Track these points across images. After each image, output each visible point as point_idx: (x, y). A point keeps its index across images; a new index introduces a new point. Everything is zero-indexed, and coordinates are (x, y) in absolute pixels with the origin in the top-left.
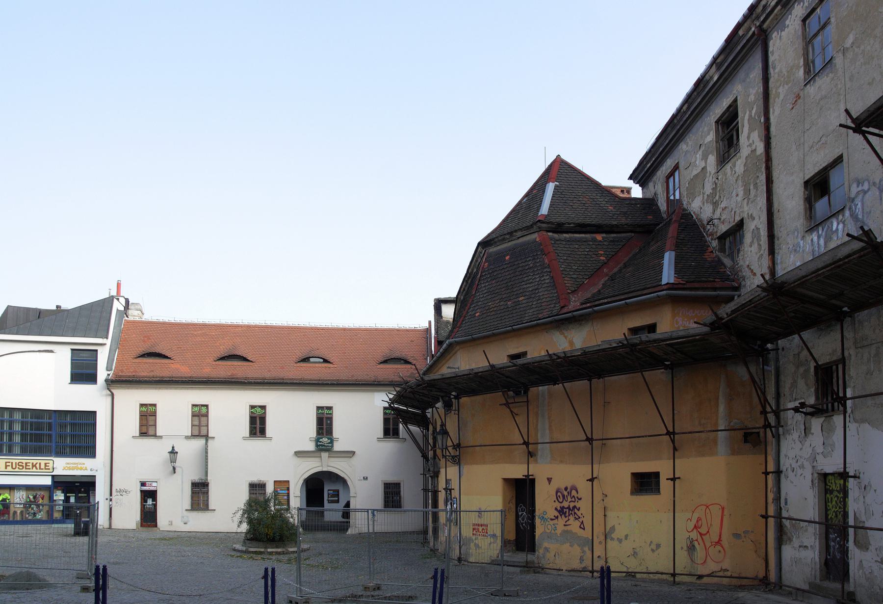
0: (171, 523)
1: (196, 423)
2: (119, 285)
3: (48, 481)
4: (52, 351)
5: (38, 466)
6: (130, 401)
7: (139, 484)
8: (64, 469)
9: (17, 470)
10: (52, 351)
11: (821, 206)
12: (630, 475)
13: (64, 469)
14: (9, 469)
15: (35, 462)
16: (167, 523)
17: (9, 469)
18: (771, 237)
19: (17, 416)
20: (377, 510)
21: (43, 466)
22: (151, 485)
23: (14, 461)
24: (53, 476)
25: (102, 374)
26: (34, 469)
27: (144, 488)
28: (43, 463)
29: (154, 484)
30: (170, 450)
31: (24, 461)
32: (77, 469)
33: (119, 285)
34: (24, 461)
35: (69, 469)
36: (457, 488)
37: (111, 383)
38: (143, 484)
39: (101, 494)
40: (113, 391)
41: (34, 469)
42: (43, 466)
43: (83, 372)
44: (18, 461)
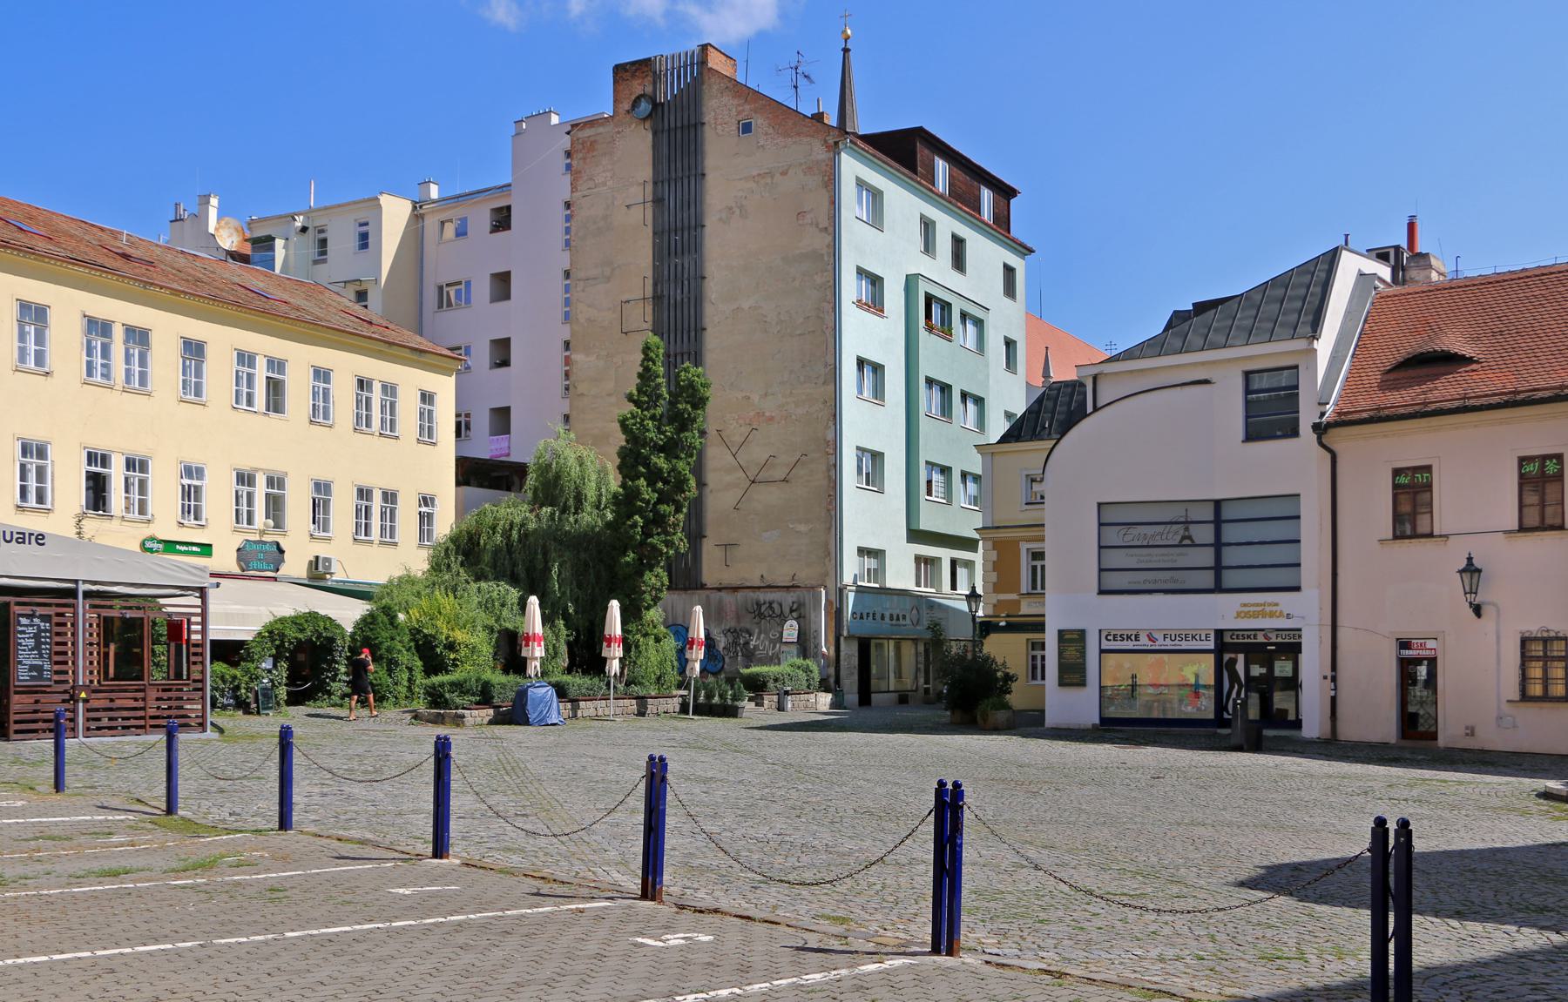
0: (1471, 732)
1: (1406, 508)
2: (1411, 227)
4: (1206, 382)
6: (1374, 460)
7: (1394, 646)
8: (1238, 615)
10: (1206, 382)
12: (487, 413)
13: (1238, 615)
16: (1462, 731)
18: (1498, 638)
19: (84, 613)
22: (1422, 647)
27: (1406, 653)
29: (1431, 644)
30: (1463, 564)
32: (1264, 614)
33: (1411, 227)
35: (1247, 615)
38: (1404, 644)
39: (1312, 664)
43: (1271, 411)
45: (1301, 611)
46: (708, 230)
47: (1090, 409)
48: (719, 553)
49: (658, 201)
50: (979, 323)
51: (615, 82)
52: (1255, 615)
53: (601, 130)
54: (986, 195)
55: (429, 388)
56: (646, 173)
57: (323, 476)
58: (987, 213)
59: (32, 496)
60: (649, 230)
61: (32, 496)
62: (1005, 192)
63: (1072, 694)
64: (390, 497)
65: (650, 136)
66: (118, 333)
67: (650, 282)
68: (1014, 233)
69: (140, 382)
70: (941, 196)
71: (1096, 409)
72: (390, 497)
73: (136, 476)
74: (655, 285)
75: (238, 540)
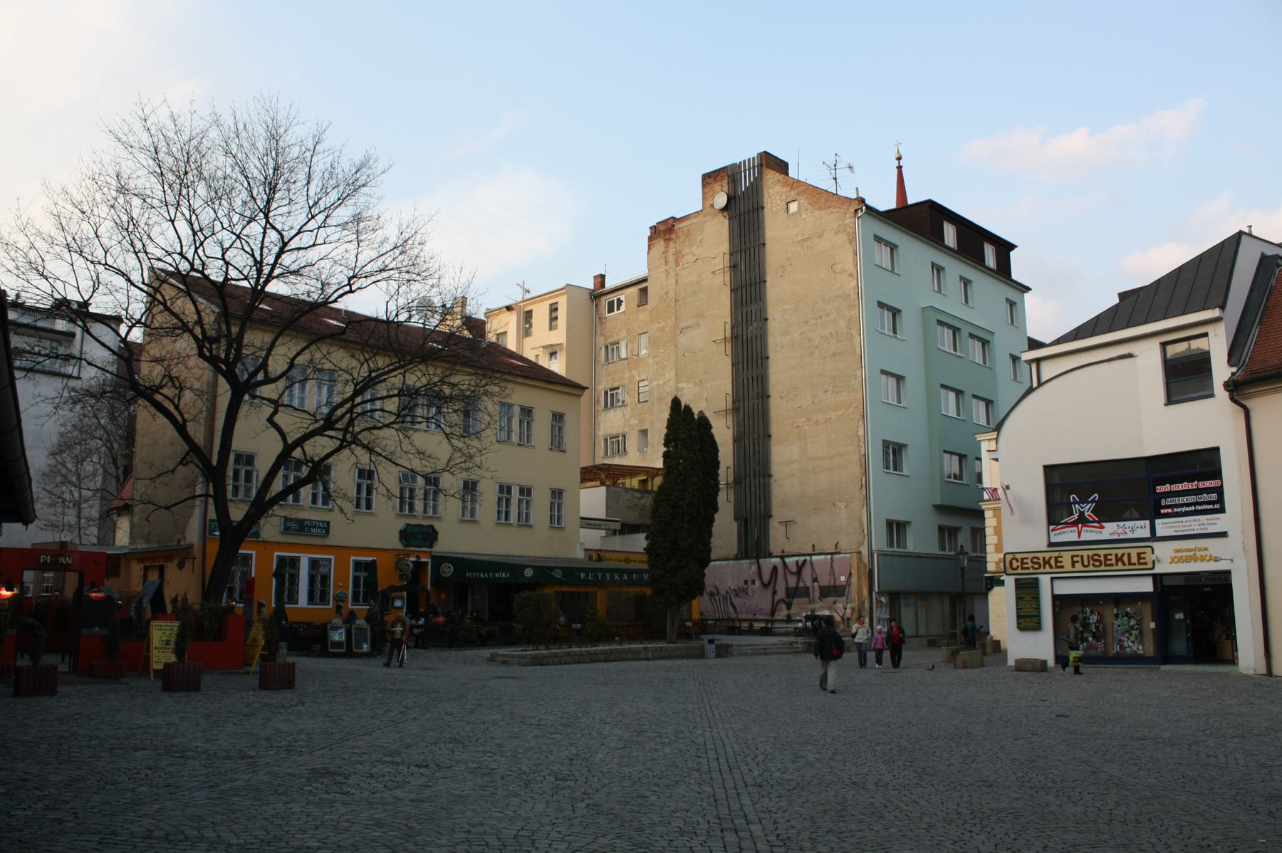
3: (1146, 586)
4: (1130, 356)
5: (1052, 562)
9: (1091, 568)
10: (1130, 356)
11: (294, 526)
14: (1079, 567)
15: (1120, 552)
17: (1079, 567)
20: (908, 594)
21: (1134, 560)
23: (1085, 554)
24: (1154, 576)
25: (1221, 371)
26: (1120, 566)
28: (1134, 553)
31: (1102, 553)
34: (1102, 553)
35: (1181, 560)
36: (796, 559)
37: (1236, 389)
40: (1244, 402)
41: (1120, 566)
42: (1134, 560)
43: (1185, 377)
44: (1091, 553)
45: (1230, 554)
46: (768, 284)
47: (1035, 385)
48: (782, 529)
49: (733, 267)
50: (985, 343)
51: (704, 186)
52: (1188, 560)
53: (694, 220)
54: (989, 251)
55: (559, 410)
56: (725, 247)
57: (557, 486)
58: (990, 261)
59: (363, 503)
60: (728, 289)
61: (363, 503)
62: (1004, 248)
63: (1029, 637)
64: (526, 491)
65: (727, 222)
66: (516, 410)
67: (728, 327)
68: (1014, 277)
69: (526, 440)
70: (991, 270)
71: (1040, 384)
72: (526, 491)
73: (365, 482)
74: (732, 328)
75: (401, 524)
